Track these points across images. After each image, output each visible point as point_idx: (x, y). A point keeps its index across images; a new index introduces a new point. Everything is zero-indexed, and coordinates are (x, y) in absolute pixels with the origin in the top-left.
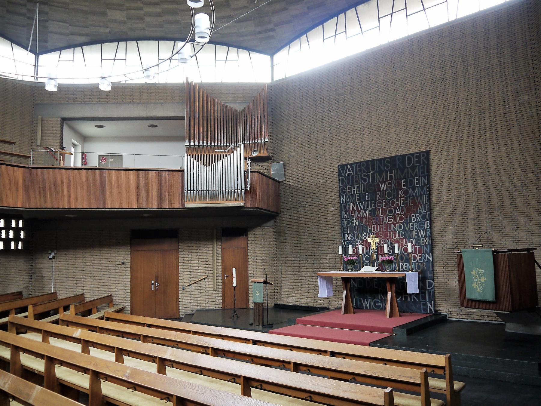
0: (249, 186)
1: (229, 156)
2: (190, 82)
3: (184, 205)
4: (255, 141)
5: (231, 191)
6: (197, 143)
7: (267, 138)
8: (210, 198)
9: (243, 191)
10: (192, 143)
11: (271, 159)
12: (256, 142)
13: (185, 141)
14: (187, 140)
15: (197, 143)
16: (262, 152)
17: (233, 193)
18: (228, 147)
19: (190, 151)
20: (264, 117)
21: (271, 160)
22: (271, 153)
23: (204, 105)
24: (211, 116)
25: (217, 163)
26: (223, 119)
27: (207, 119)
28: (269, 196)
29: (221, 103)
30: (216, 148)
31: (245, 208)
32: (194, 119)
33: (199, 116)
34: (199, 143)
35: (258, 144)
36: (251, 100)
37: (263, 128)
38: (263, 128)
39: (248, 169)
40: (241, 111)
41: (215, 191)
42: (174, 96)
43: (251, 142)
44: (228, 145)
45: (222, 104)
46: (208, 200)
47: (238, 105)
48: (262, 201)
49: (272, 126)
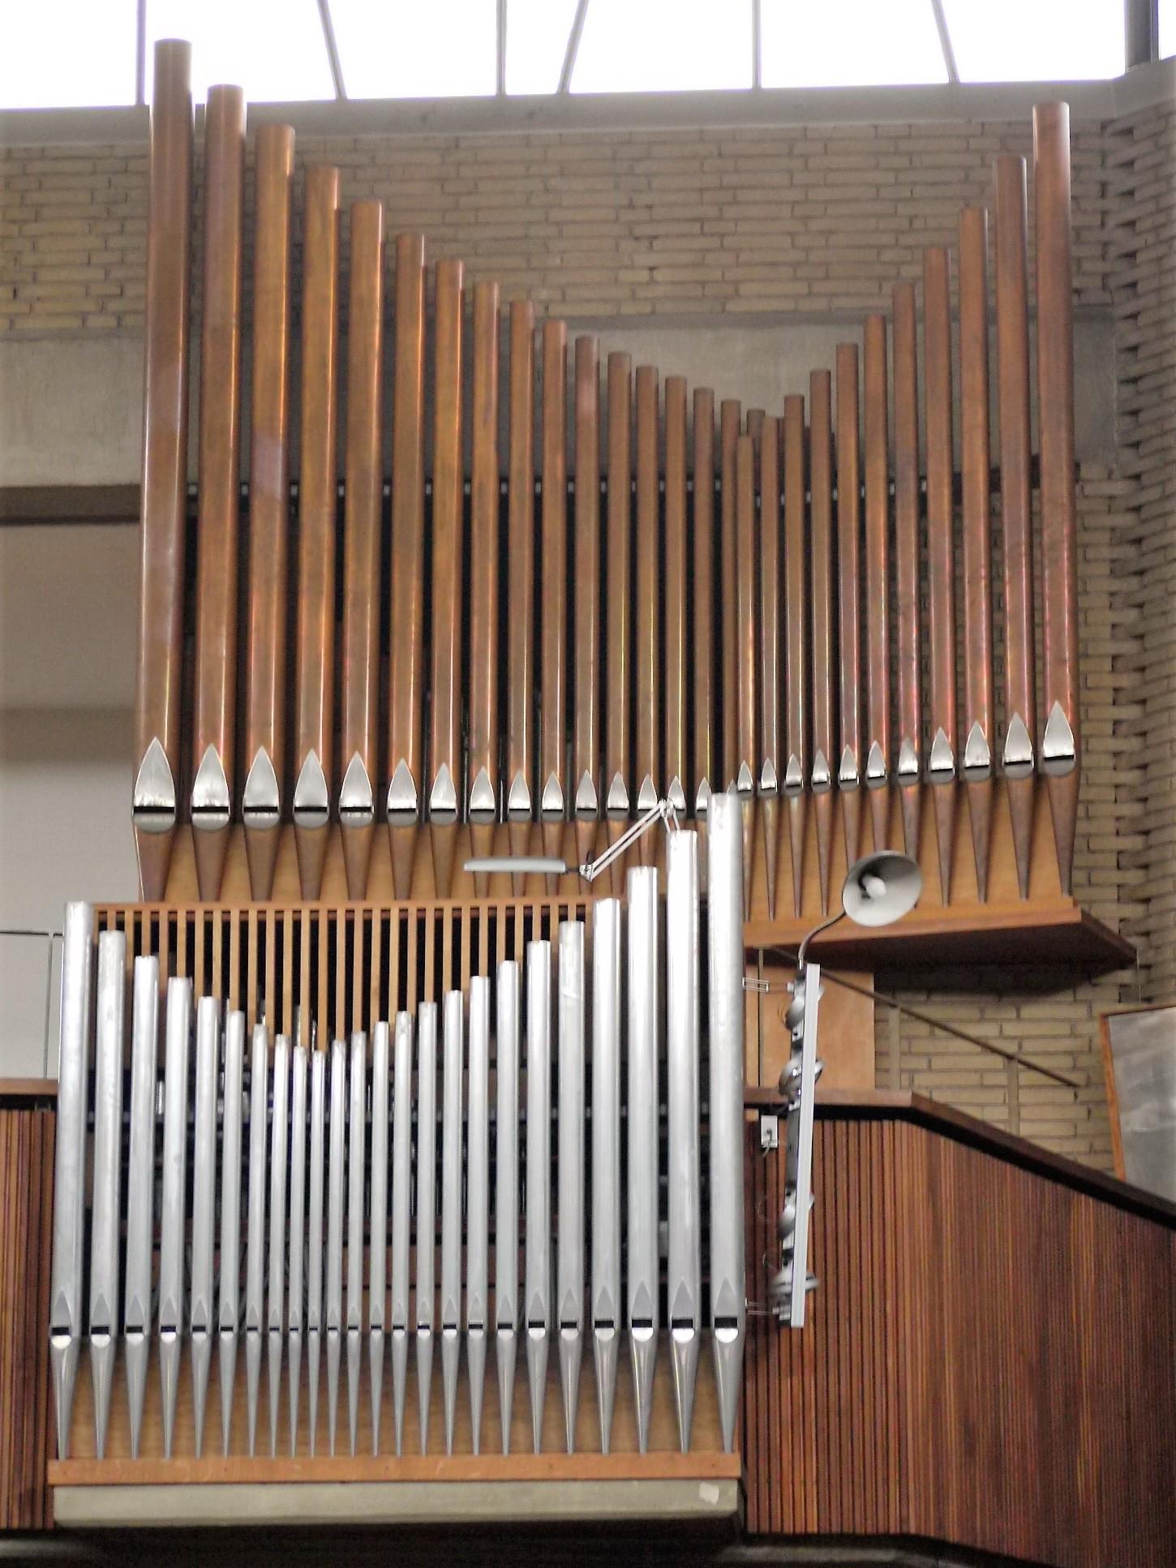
0: (796, 1279)
1: (571, 933)
2: (199, 96)
3: (39, 1496)
4: (924, 757)
5: (587, 1339)
6: (262, 787)
7: (1059, 715)
8: (343, 1424)
9: (726, 1336)
10: (210, 788)
11: (1125, 960)
12: (942, 761)
13: (127, 757)
14: (157, 754)
15: (262, 787)
16: (1006, 875)
17: (605, 1360)
18: (615, 826)
19: (184, 872)
20: (1034, 481)
21: (1126, 976)
22: (1124, 895)
23: (355, 359)
24: (429, 480)
25: (428, 1011)
26: (570, 501)
27: (386, 506)
28: (1071, 1399)
29: (543, 325)
30: (482, 833)
31: (759, 1539)
32: (244, 506)
33: (293, 480)
34: (288, 780)
35: (925, 789)
36: (887, 288)
37: (1016, 597)
38: (1016, 597)
39: (788, 1086)
40: (776, 410)
41: (399, 1336)
42: (29, 259)
43: (876, 770)
44: (618, 799)
45: (563, 335)
46: (323, 1441)
47: (741, 343)
48: (970, 1450)
49: (1133, 583)
